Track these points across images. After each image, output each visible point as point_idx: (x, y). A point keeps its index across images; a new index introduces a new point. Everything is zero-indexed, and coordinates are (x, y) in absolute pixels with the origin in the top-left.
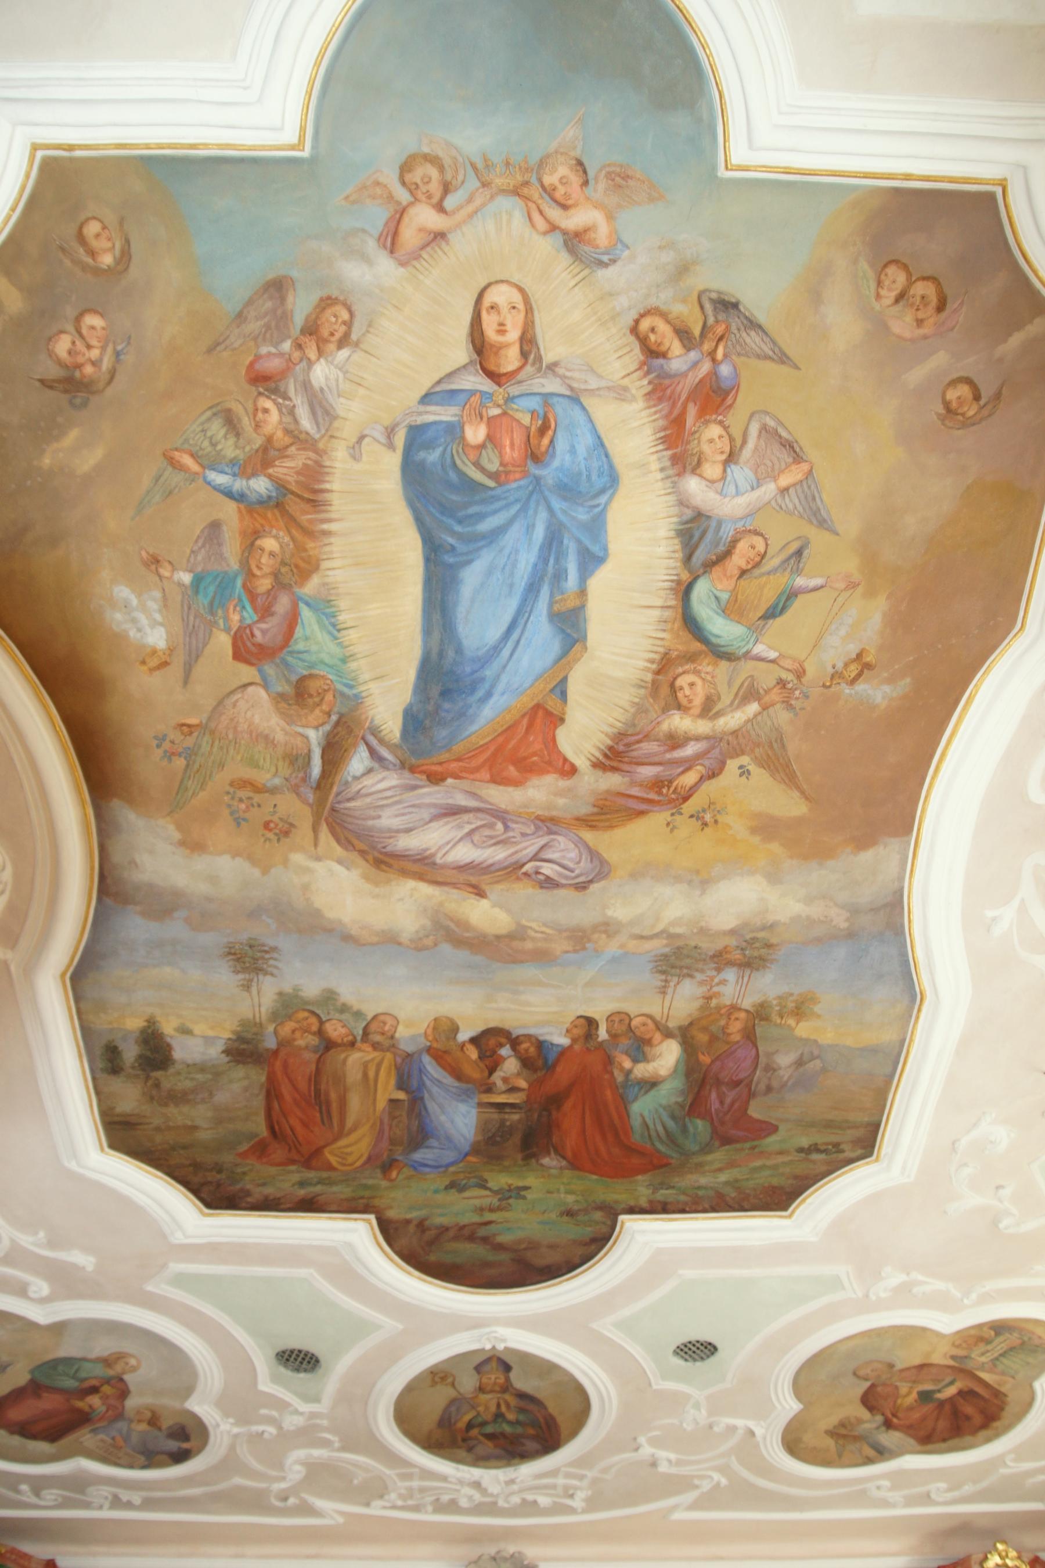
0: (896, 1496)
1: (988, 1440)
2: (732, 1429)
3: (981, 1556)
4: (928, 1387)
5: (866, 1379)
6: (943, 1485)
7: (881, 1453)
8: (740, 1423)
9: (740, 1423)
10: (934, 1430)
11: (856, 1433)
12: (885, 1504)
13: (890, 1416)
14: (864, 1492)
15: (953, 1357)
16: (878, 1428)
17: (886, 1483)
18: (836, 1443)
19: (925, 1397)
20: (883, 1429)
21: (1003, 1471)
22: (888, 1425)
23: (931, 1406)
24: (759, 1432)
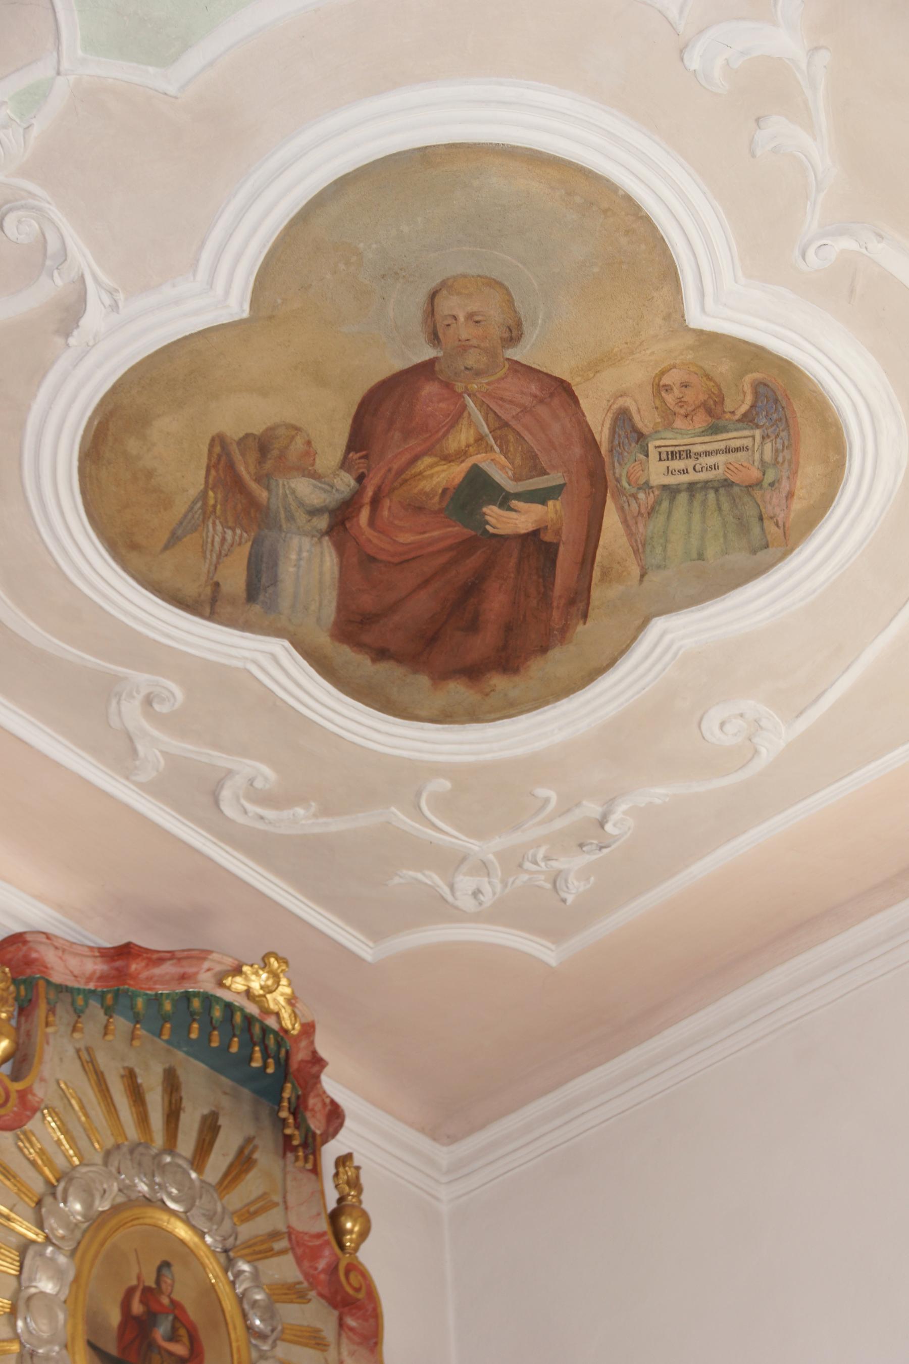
0: (157, 746)
1: (445, 717)
2: (39, 258)
3: (229, 962)
4: (502, 477)
5: (435, 338)
6: (266, 775)
7: (248, 599)
8: (82, 256)
9: (82, 256)
10: (393, 608)
11: (263, 495)
12: (122, 754)
13: (369, 493)
14: (108, 689)
15: (622, 418)
16: (314, 512)
17: (175, 692)
18: (204, 495)
19: (478, 489)
20: (323, 523)
21: (399, 817)
22: (340, 520)
23: (457, 531)
24: (94, 318)
